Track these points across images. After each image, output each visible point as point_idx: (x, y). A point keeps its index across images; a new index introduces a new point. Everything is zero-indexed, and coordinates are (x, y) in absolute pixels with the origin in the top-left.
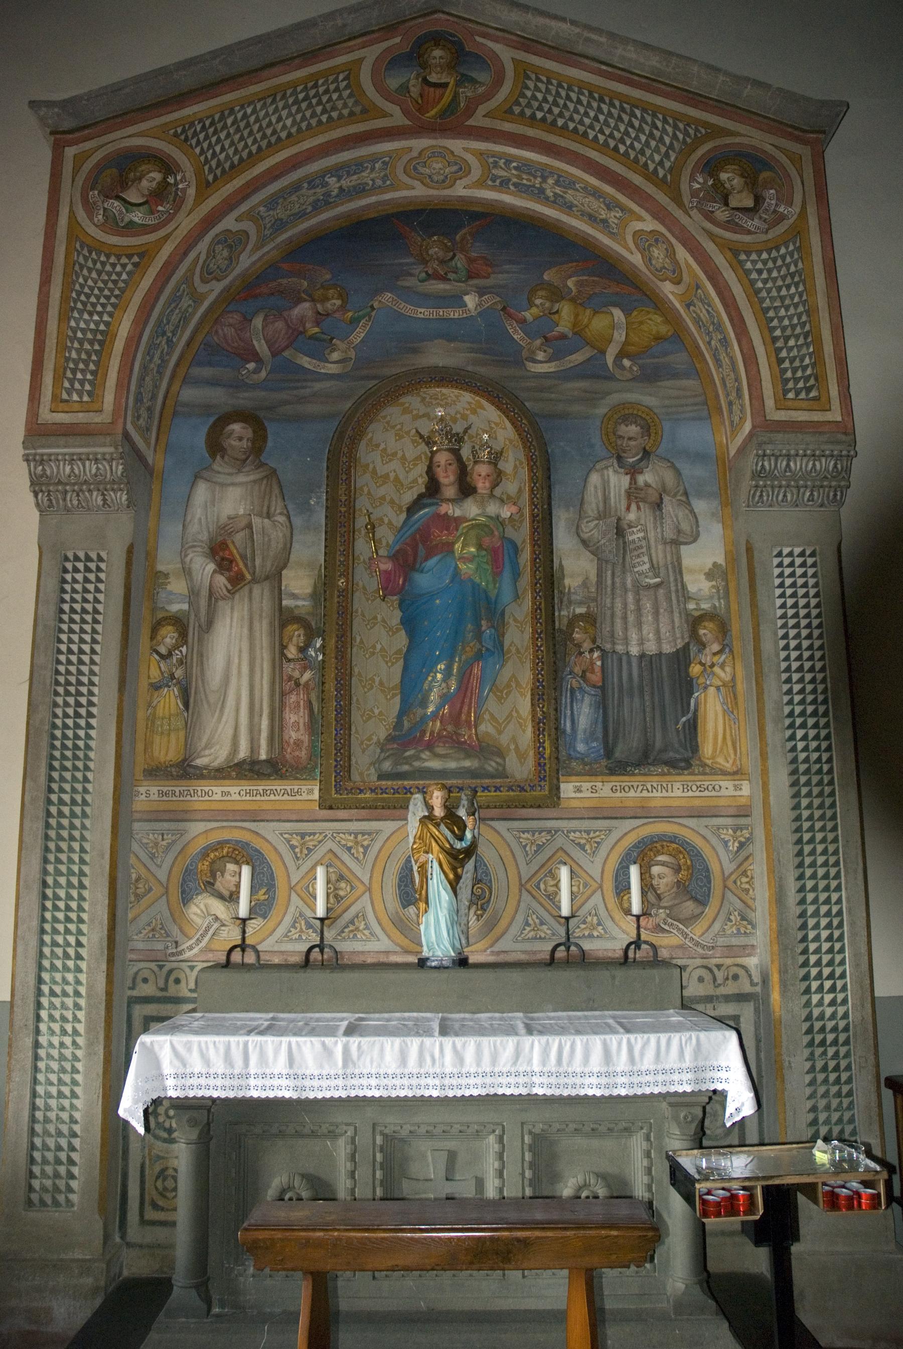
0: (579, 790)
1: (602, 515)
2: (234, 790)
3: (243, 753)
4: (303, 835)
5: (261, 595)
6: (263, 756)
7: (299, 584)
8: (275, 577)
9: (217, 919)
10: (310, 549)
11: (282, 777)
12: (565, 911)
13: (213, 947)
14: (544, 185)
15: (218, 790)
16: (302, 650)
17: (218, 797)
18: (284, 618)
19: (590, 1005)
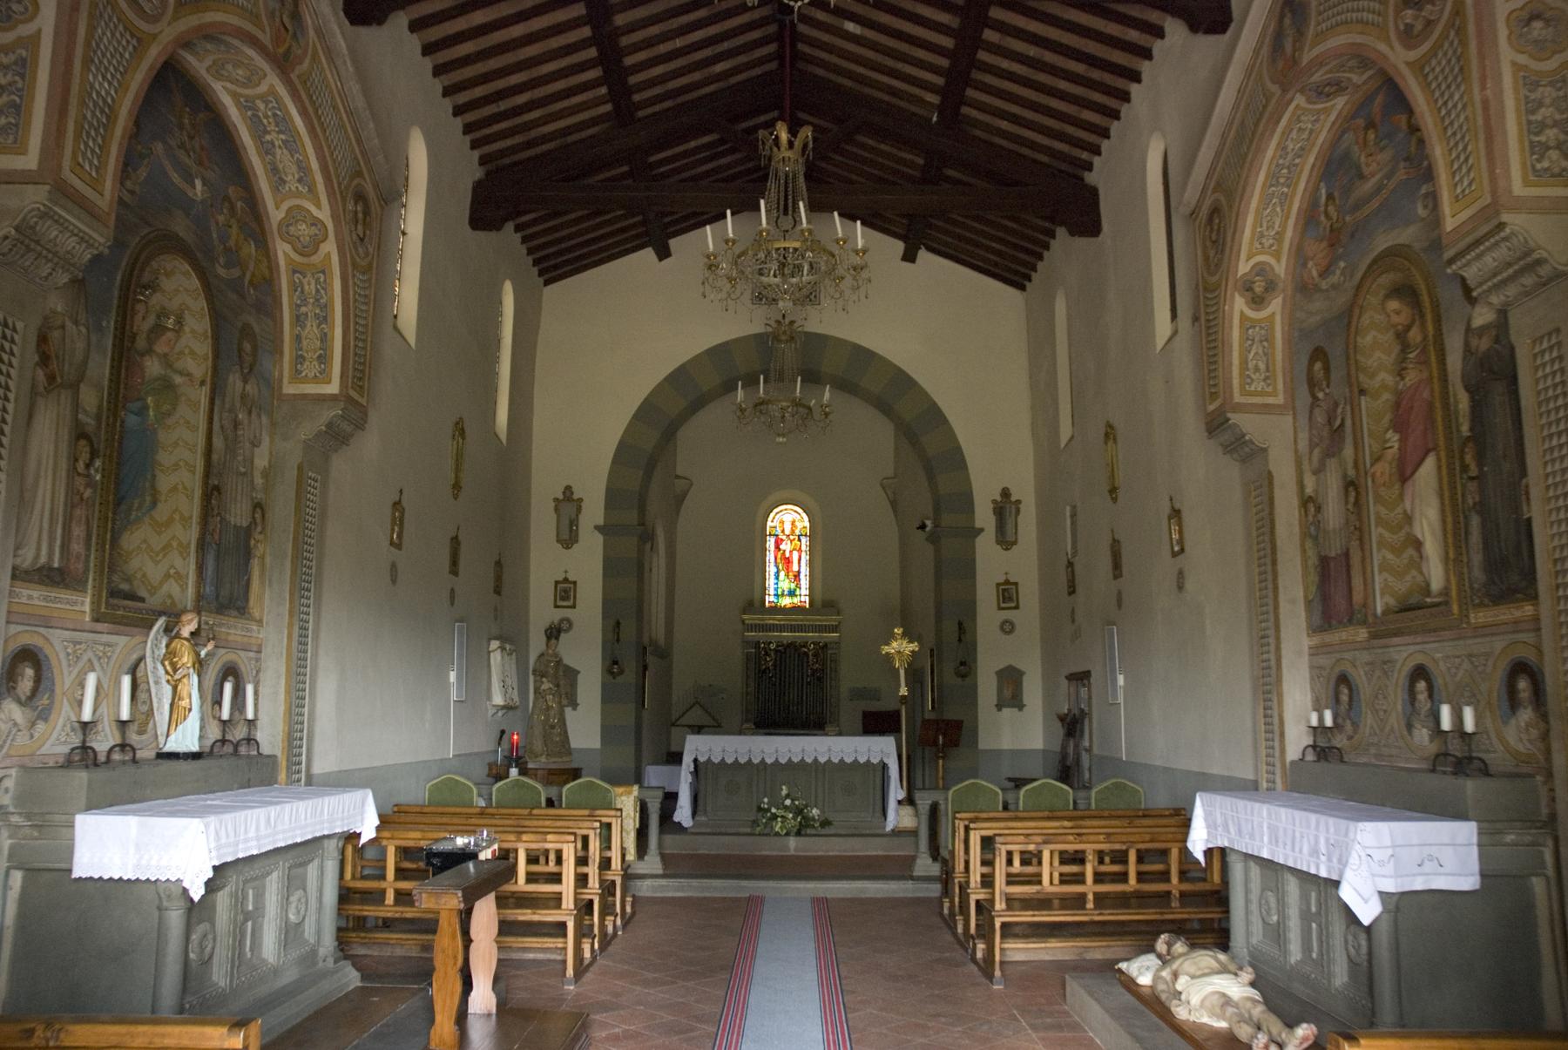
0: (1011, 687)
1: (230, 411)
2: (35, 594)
3: (43, 560)
4: (76, 643)
5: (65, 396)
6: (56, 565)
7: (90, 399)
8: (75, 387)
9: (15, 724)
10: (100, 368)
11: (67, 587)
12: (250, 716)
13: (12, 752)
14: (1548, 101)
15: (25, 592)
16: (88, 466)
17: (24, 600)
18: (80, 434)
19: (248, 784)
